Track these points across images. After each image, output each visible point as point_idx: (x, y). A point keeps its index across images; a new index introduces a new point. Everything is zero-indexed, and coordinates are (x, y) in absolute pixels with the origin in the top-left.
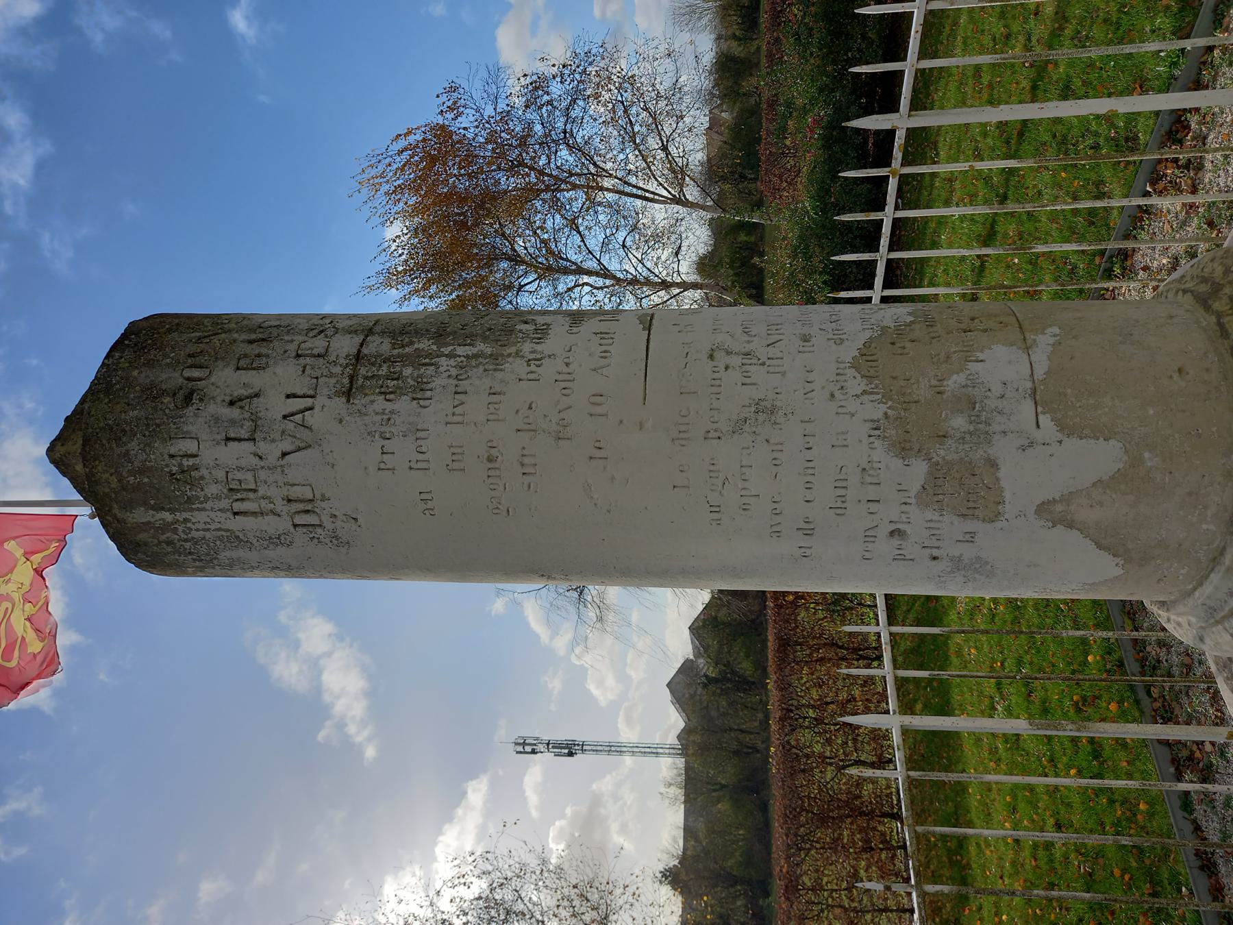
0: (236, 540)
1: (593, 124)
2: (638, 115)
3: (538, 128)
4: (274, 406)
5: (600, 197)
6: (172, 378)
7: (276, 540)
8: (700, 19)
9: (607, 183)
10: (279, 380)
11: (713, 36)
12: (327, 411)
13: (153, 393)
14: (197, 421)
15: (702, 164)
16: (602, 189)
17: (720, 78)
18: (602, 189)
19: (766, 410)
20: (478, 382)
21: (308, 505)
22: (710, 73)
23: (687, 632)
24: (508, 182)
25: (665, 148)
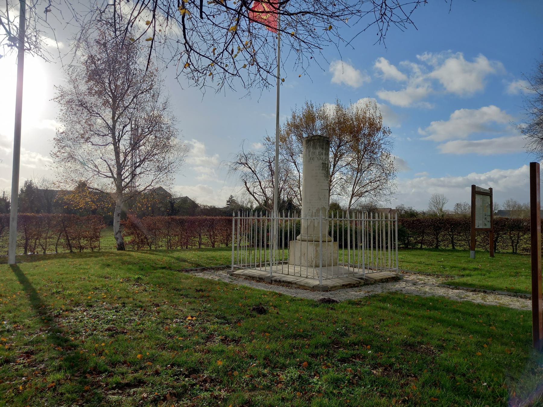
0: (309, 152)
1: (374, 172)
2: (379, 184)
3: (375, 156)
4: (322, 157)
5: (355, 173)
6: (324, 147)
7: (309, 156)
8: (434, 206)
9: (359, 174)
10: (324, 157)
11: (425, 211)
12: (321, 162)
13: (323, 145)
14: (321, 150)
15: (375, 205)
16: (358, 173)
17: (408, 213)
18: (358, 173)
19: (320, 199)
20: (323, 175)
21: (313, 159)
22: (411, 209)
23: (184, 196)
24: (361, 147)
25: (367, 191)
